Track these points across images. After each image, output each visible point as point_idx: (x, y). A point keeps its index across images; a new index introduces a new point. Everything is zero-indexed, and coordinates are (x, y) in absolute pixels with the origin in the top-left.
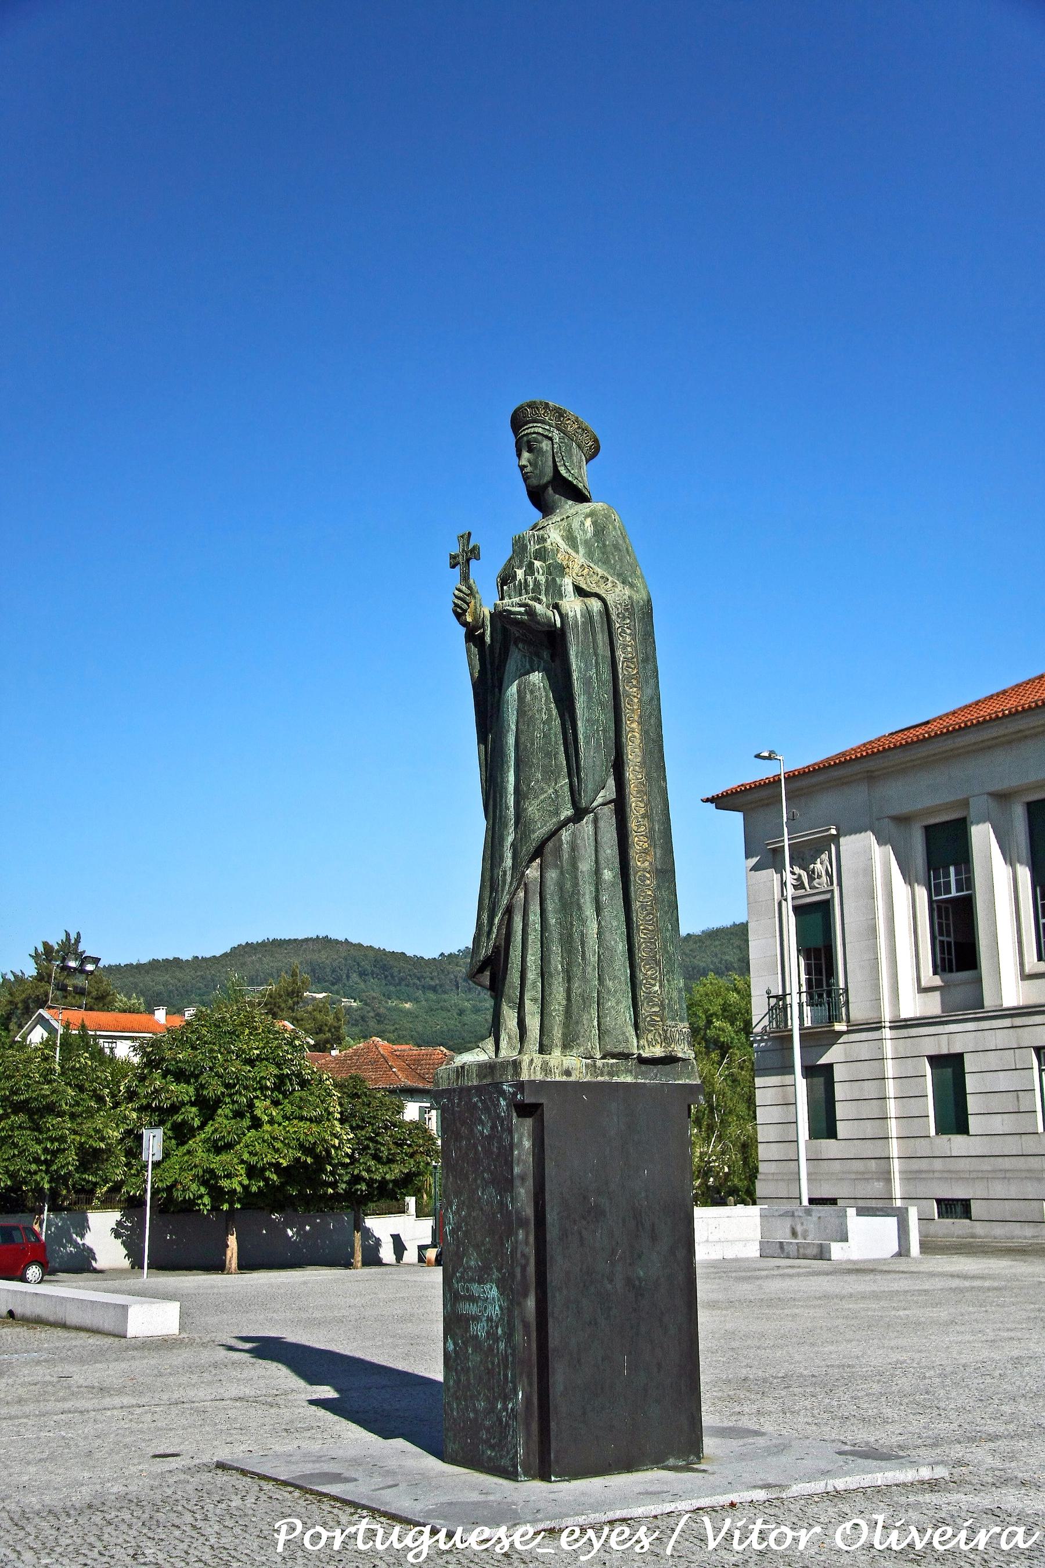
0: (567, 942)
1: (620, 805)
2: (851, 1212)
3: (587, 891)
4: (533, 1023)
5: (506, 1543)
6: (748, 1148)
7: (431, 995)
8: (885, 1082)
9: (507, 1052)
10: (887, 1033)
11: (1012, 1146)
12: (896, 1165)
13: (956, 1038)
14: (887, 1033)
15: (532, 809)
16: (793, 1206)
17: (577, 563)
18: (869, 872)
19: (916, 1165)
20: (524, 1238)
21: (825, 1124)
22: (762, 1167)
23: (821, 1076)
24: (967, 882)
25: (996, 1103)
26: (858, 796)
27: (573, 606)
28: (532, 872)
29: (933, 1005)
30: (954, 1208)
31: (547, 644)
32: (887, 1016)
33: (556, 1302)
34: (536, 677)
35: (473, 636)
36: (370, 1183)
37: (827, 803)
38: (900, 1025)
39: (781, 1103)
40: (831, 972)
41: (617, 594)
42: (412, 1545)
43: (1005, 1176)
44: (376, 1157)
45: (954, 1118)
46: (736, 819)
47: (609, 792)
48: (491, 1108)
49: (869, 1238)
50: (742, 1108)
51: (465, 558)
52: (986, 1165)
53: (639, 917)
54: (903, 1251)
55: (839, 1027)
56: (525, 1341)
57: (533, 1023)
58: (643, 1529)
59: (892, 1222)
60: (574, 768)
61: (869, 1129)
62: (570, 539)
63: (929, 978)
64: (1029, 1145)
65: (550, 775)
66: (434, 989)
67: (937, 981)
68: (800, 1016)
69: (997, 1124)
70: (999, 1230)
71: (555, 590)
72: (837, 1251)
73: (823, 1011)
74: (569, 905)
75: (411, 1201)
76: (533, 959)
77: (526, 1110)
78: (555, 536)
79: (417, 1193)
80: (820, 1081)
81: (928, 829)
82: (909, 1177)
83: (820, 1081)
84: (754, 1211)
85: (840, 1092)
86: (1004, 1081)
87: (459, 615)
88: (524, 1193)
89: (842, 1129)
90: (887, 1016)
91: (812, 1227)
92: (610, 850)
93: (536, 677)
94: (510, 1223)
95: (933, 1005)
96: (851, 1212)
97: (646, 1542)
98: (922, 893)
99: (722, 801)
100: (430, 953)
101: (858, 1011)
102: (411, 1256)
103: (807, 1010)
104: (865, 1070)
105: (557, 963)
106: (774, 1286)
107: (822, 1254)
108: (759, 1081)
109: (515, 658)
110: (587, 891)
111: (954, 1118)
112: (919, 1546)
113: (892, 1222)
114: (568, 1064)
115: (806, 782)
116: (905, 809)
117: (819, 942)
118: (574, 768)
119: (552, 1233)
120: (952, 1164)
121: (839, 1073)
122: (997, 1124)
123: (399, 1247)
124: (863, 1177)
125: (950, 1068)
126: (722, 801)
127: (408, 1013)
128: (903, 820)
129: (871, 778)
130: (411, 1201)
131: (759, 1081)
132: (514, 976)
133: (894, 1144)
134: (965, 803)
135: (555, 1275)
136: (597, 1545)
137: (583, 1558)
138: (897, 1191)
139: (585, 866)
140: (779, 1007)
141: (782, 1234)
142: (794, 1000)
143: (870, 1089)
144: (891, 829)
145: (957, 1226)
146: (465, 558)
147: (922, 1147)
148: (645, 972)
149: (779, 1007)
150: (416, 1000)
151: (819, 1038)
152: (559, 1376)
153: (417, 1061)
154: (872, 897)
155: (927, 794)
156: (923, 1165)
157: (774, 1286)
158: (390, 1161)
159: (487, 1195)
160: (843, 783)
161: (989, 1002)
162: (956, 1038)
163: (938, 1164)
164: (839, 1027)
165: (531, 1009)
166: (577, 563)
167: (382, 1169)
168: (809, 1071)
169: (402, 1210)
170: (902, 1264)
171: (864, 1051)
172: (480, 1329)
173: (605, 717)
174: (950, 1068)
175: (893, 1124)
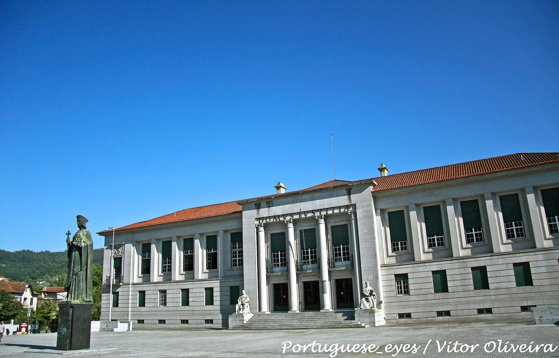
0: (78, 286)
1: (87, 269)
2: (119, 322)
3: (81, 279)
4: (73, 296)
5: (365, 350)
6: (99, 308)
7: (11, 263)
8: (129, 296)
9: (69, 300)
10: (131, 286)
11: (153, 309)
12: (130, 313)
13: (144, 288)
14: (131, 286)
15: (75, 269)
16: (107, 321)
17: (84, 238)
18: (130, 252)
19: (134, 313)
20: (70, 323)
21: (116, 304)
22: (102, 313)
23: (116, 294)
24: (149, 256)
25: (151, 301)
26: (129, 236)
27: (83, 244)
28: (74, 277)
29: (140, 280)
30: (141, 322)
31: (79, 249)
32: (131, 283)
33: (74, 329)
34: (77, 252)
35: (68, 244)
36: (5, 316)
37: (123, 237)
38: (133, 284)
39: (107, 299)
40: (120, 272)
41: (89, 243)
42: (331, 351)
43: (151, 315)
44: (7, 310)
45: (142, 303)
46: (103, 237)
47: (85, 268)
48: (67, 307)
49: (122, 327)
50: (98, 299)
51: (69, 234)
52: (148, 313)
53: (88, 284)
54: (129, 330)
55: (121, 284)
56: (69, 335)
57: (73, 296)
58: (415, 345)
59: (127, 324)
60: (81, 265)
61: (125, 305)
62: (83, 235)
63: (140, 275)
64: (156, 309)
65: (78, 265)
66: (12, 261)
67: (142, 276)
68: (113, 281)
69: (151, 305)
70: (149, 326)
71: (81, 242)
72: (115, 330)
73: (118, 280)
74: (79, 282)
75: (13, 321)
76: (73, 288)
77: (71, 307)
78: (81, 234)
79: (14, 319)
80: (116, 295)
81: (143, 244)
82: (132, 315)
83: (116, 295)
84: (99, 322)
85: (120, 297)
86: (152, 296)
87: (67, 241)
88: (70, 317)
89: (119, 305)
90: (131, 283)
91: (110, 326)
92: (85, 275)
93: (77, 252)
94: (68, 320)
95: (140, 280)
96: (119, 322)
97: (416, 350)
98: (140, 257)
99: (101, 234)
100: (12, 250)
101: (125, 281)
102: (11, 333)
103: (114, 280)
104: (125, 293)
105: (77, 289)
106: (102, 335)
107: (112, 330)
108: (103, 295)
109: (74, 249)
110: (81, 279)
111: (142, 303)
112: (514, 351)
113: (127, 324)
114: (77, 302)
115: (119, 232)
116: (139, 240)
117: (118, 266)
118: (81, 265)
119: (74, 322)
120: (141, 313)
121: (120, 294)
122: (151, 305)
123: (8, 332)
124: (123, 315)
125: (142, 294)
126: (101, 234)
127: (3, 267)
128: (138, 242)
129: (132, 233)
130: (13, 321)
131: (103, 295)
132: (71, 290)
133: (130, 309)
134: (151, 240)
135: (74, 326)
136: (398, 351)
137: (393, 355)
138: (130, 318)
139: (81, 277)
140: (109, 279)
141: (105, 327)
142: (112, 278)
143: (126, 297)
144: (135, 243)
145: (141, 325)
146: (69, 234)
147: (135, 309)
148: (88, 290)
149: (109, 279)
150: (6, 264)
151: (116, 286)
152: (73, 339)
153: (16, 285)
154: (130, 257)
155: (143, 237)
156: (135, 313)
157: (102, 335)
158: (10, 311)
159: (65, 317)
160: (126, 233)
161: (151, 281)
162: (144, 288)
163: (138, 313)
164: (121, 284)
165: (73, 294)
166: (84, 238)
167: (8, 312)
168: (113, 293)
169: (10, 323)
170: (129, 332)
171: (126, 289)
172: (63, 334)
173: (86, 259)
174: (142, 294)
175: (130, 304)
